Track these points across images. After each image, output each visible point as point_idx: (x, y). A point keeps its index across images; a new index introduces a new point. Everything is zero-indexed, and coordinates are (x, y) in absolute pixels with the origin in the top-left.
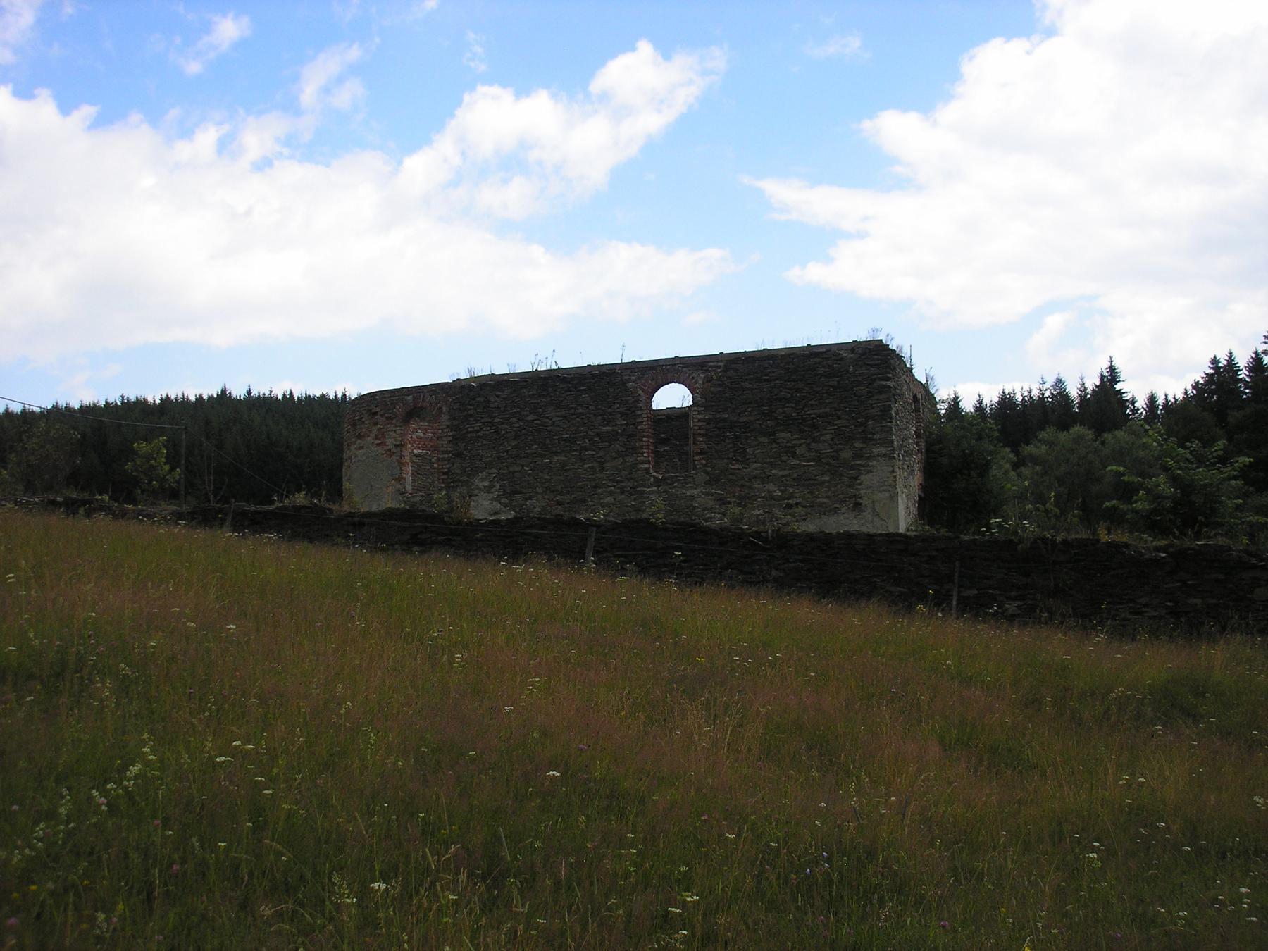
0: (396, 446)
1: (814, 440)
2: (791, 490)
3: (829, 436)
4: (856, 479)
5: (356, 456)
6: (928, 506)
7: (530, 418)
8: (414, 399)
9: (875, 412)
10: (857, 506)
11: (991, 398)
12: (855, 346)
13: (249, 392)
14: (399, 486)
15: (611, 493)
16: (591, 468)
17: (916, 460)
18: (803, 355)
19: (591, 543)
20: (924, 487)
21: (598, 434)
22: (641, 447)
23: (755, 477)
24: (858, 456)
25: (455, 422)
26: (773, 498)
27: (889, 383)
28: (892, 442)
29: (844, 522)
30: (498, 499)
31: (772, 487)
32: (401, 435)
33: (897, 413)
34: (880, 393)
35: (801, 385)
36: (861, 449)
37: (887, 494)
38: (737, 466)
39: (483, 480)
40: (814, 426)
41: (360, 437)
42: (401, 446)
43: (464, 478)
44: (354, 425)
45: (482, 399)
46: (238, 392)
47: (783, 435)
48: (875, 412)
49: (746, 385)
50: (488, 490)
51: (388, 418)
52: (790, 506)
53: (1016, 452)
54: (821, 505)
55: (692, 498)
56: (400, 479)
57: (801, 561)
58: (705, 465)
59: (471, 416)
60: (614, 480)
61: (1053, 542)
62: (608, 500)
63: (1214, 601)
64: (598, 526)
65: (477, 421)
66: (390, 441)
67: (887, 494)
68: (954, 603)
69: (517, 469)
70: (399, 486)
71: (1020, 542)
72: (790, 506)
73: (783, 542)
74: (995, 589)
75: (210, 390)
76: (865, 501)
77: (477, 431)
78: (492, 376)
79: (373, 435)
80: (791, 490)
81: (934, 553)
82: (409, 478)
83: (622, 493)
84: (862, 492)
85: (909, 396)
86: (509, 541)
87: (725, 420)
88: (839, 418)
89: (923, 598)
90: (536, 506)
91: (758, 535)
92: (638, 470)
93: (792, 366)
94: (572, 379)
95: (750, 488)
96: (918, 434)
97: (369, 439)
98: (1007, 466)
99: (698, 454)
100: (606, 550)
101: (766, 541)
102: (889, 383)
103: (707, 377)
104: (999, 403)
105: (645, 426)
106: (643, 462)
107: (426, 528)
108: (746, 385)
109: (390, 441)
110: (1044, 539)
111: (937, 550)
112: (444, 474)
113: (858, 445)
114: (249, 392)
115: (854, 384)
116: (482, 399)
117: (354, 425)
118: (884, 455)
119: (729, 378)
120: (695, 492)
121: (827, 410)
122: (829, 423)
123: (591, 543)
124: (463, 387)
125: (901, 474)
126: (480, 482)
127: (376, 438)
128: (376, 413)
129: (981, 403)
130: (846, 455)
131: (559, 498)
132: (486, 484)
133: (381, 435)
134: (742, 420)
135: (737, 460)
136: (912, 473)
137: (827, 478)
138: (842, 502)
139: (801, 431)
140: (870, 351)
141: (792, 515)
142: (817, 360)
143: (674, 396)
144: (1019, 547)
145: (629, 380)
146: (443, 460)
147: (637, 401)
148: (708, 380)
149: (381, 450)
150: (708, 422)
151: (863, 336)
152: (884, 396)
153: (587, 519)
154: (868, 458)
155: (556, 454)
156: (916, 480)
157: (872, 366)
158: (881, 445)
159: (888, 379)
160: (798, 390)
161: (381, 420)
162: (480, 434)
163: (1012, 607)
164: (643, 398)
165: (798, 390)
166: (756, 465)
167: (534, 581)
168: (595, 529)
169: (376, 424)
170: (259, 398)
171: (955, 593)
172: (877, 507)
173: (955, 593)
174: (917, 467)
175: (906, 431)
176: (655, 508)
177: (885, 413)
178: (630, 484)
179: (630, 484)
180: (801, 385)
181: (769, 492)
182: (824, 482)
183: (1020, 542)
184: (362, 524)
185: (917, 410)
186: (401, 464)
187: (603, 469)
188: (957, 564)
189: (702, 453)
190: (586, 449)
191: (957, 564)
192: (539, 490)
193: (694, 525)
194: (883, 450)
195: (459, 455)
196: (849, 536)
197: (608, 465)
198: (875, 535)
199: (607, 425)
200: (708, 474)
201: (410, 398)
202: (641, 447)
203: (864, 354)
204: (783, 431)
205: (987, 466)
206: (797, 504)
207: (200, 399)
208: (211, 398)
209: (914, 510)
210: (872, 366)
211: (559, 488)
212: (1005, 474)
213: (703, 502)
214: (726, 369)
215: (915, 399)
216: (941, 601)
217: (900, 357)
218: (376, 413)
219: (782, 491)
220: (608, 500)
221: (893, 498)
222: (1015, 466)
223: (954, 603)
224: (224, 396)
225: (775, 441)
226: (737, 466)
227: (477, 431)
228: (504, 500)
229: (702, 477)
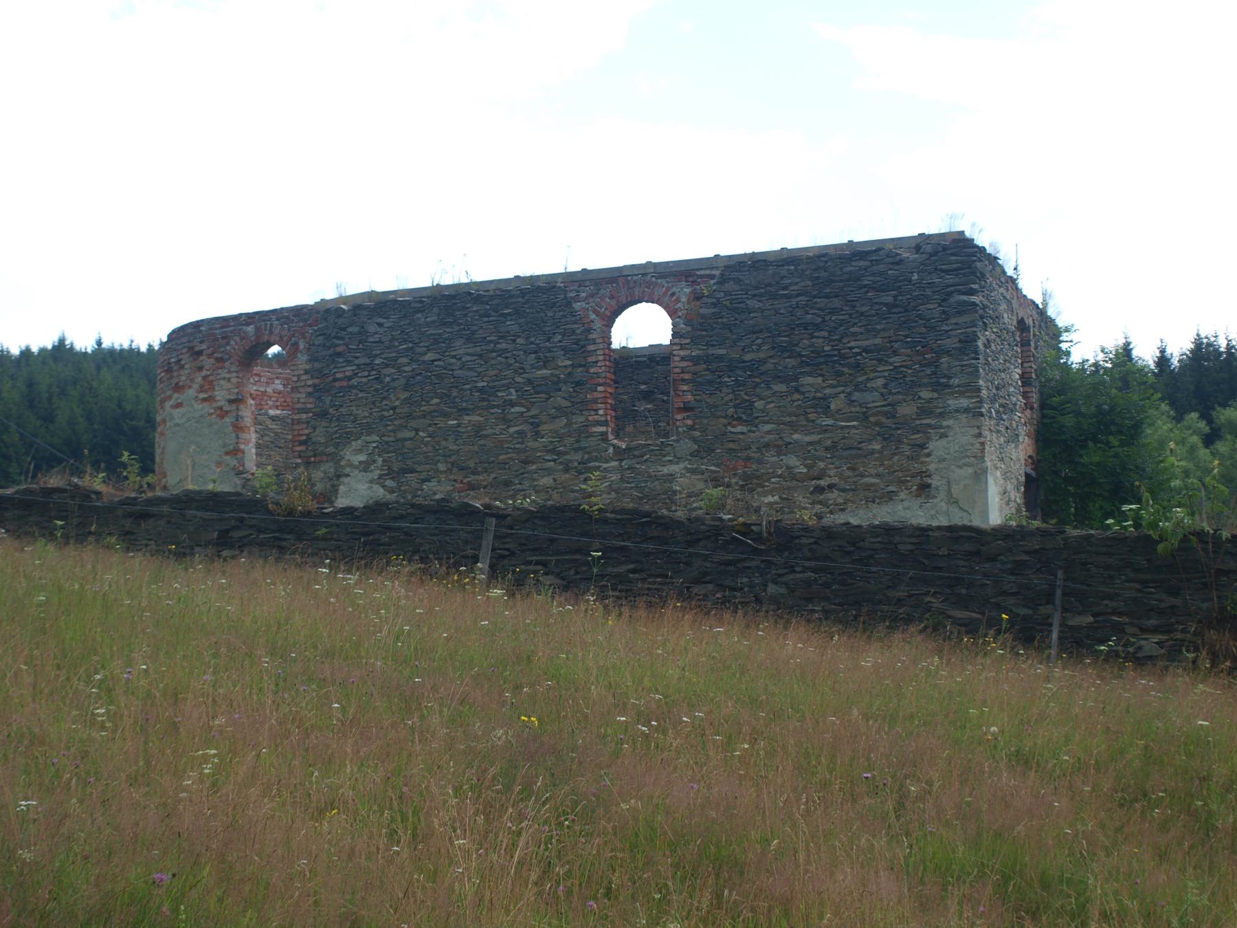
0: (231, 402)
1: (857, 388)
2: (822, 465)
3: (880, 382)
4: (922, 446)
5: (172, 418)
6: (1039, 488)
7: (429, 356)
8: (258, 329)
9: (951, 343)
10: (924, 488)
11: (1179, 347)
12: (921, 243)
13: (99, 343)
14: (234, 462)
15: (549, 471)
16: (519, 433)
17: (1022, 420)
18: (841, 257)
19: (488, 541)
20: (1035, 462)
21: (530, 382)
22: (595, 401)
23: (767, 445)
24: (925, 412)
25: (317, 365)
26: (794, 478)
27: (974, 299)
28: (979, 390)
29: (910, 512)
30: (380, 480)
31: (792, 461)
32: (239, 385)
33: (987, 345)
34: (960, 313)
35: (837, 303)
36: (930, 401)
37: (970, 470)
38: (739, 429)
39: (360, 451)
40: (858, 367)
41: (178, 388)
42: (237, 401)
43: (331, 449)
44: (169, 371)
45: (354, 329)
46: (83, 342)
47: (810, 380)
48: (951, 343)
49: (753, 303)
50: (365, 467)
51: (220, 360)
52: (820, 490)
53: (1206, 416)
54: (868, 487)
55: (671, 477)
56: (236, 452)
57: (814, 570)
58: (692, 428)
59: (339, 354)
60: (552, 451)
61: (1216, 538)
62: (546, 481)
63: (830, 422)
64: (501, 517)
65: (349, 362)
66: (221, 395)
67: (970, 470)
68: (1055, 635)
69: (407, 434)
70: (234, 462)
71: (1162, 539)
72: (820, 490)
73: (785, 539)
74: (1120, 614)
75: (41, 339)
76: (935, 481)
77: (350, 378)
78: (371, 295)
79: (196, 386)
80: (822, 465)
81: (1024, 557)
82: (251, 451)
83: (566, 470)
84: (932, 467)
85: (1009, 320)
86: (366, 539)
87: (720, 358)
88: (895, 353)
89: (994, 623)
90: (438, 490)
91: (746, 529)
92: (591, 435)
93: (823, 274)
94: (492, 297)
95: (760, 462)
96: (1025, 379)
97: (191, 393)
98: (1195, 439)
99: (680, 410)
100: (513, 554)
101: (758, 538)
102: (974, 299)
103: (693, 292)
104: (1192, 351)
105: (601, 368)
106: (598, 423)
107: (242, 520)
108: (753, 303)
109: (221, 395)
110: (1200, 534)
111: (1026, 552)
112: (301, 443)
113: (925, 394)
114: (99, 343)
115: (918, 307)
116: (354, 329)
117: (169, 371)
118: (967, 410)
119: (728, 293)
120: (674, 468)
121: (878, 341)
122: (880, 361)
123: (488, 541)
124: (328, 311)
125: (993, 441)
126: (353, 455)
127: (202, 389)
128: (200, 353)
129: (1163, 351)
130: (907, 410)
131: (472, 478)
132: (363, 458)
133: (208, 385)
134: (748, 357)
135: (739, 419)
136: (1014, 438)
137: (877, 447)
138: (901, 482)
139: (839, 374)
140: (945, 248)
141: (823, 503)
142: (862, 263)
143: (643, 327)
144: (1160, 547)
145: (577, 299)
146: (299, 422)
147: (589, 331)
148: (697, 297)
149: (208, 408)
150: (695, 361)
151: (934, 225)
152: (966, 318)
153: (486, 506)
154: (942, 415)
155: (465, 411)
156: (1022, 451)
157: (946, 272)
158: (962, 394)
159: (972, 292)
160: (834, 311)
161: (208, 362)
162: (354, 382)
163: (1150, 644)
164: (598, 325)
165: (834, 311)
166: (768, 427)
167: (387, 605)
168: (494, 520)
169: (200, 369)
170: (112, 352)
171: (1056, 621)
172: (955, 490)
173: (1056, 621)
174: (1022, 431)
175: (1004, 374)
176: (600, 490)
177: (968, 342)
178: (578, 456)
179: (578, 456)
180: (837, 303)
181: (789, 468)
182: (873, 452)
183: (1162, 539)
184: (145, 516)
185: (1025, 344)
186: (238, 428)
187: (537, 435)
188: (1060, 574)
189: (686, 408)
190: (512, 404)
191: (1060, 574)
192: (442, 467)
193: (647, 514)
194: (964, 402)
195: (323, 414)
196: (888, 531)
197: (544, 428)
198: (929, 529)
199: (545, 367)
200: (695, 440)
201: (250, 329)
202: (595, 401)
203: (935, 253)
204: (810, 374)
205: (1137, 427)
206: (831, 486)
207: (26, 353)
208: (43, 351)
209: (1017, 497)
210: (946, 272)
211: (471, 464)
212: (1172, 442)
213: (686, 484)
214: (723, 280)
215: (1022, 325)
216: (1028, 635)
217: (993, 260)
218: (200, 353)
219: (809, 467)
220: (546, 481)
221: (980, 476)
222: (1209, 440)
223: (1055, 635)
224: (61, 350)
225: (797, 390)
226: (739, 429)
227: (350, 378)
228: (389, 483)
229: (687, 446)
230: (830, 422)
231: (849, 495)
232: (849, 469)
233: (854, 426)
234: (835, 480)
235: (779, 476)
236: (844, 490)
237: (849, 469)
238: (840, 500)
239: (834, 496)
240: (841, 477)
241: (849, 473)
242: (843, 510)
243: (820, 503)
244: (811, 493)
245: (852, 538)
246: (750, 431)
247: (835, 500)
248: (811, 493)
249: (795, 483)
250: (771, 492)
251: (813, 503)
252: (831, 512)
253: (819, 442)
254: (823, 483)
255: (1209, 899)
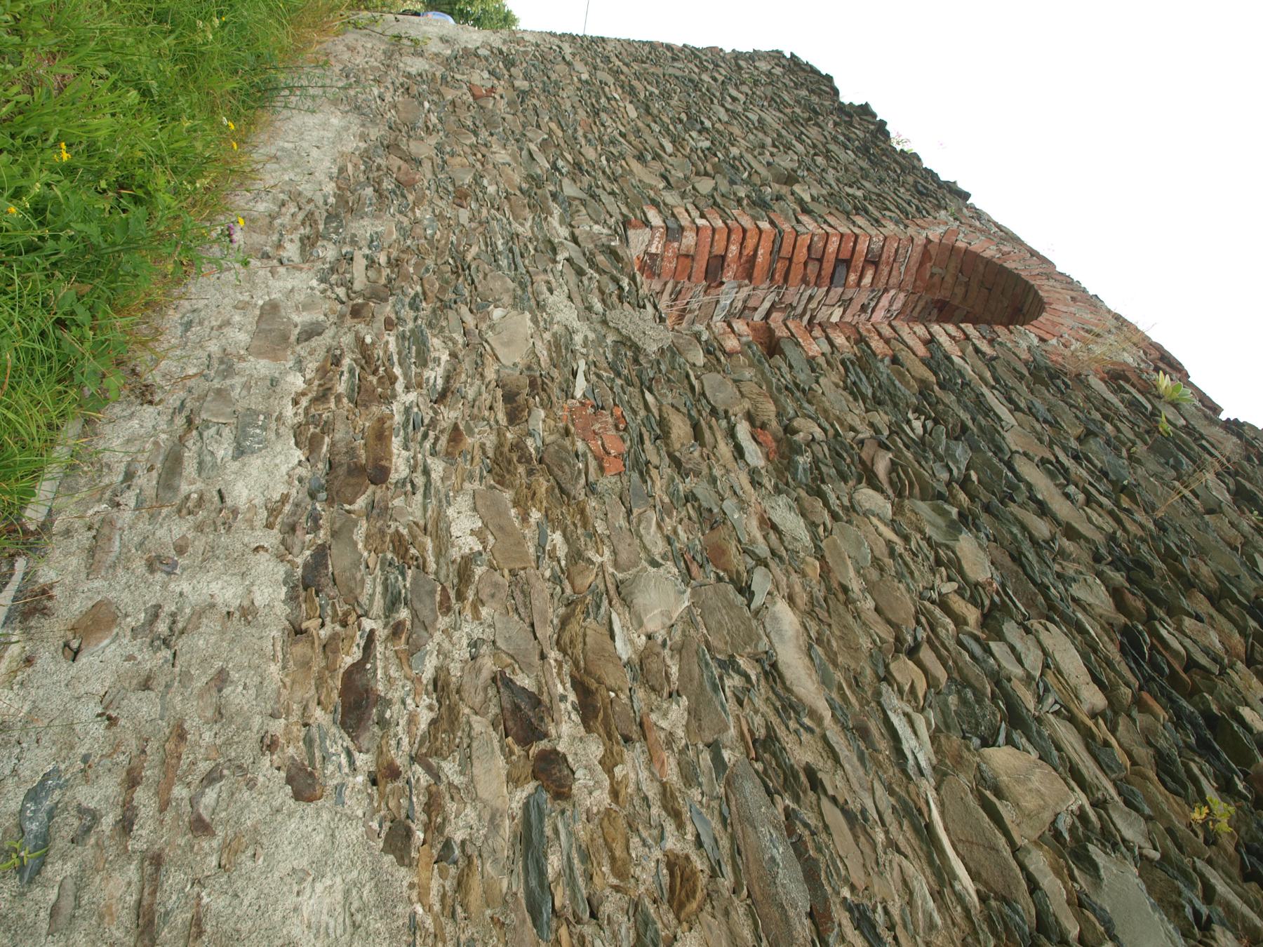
52: (524, 720)
63: (919, 749)
181: (623, 593)
219: (642, 668)
230: (919, 749)
231: (500, 876)
232: (675, 864)
233: (943, 876)
234: (591, 791)
235: (576, 556)
236: (530, 842)
237: (675, 864)
238: (462, 824)
239: (491, 786)
240: (623, 816)
241: (648, 873)
242: (397, 840)
243: (447, 719)
244: (500, 681)
245: (819, 876)
246: (753, 474)
247: (468, 793)
248: (500, 681)
249: (554, 613)
250: (492, 525)
251: (439, 685)
252: (383, 775)
253: (789, 706)
254: (566, 731)
255: (177, 100)
